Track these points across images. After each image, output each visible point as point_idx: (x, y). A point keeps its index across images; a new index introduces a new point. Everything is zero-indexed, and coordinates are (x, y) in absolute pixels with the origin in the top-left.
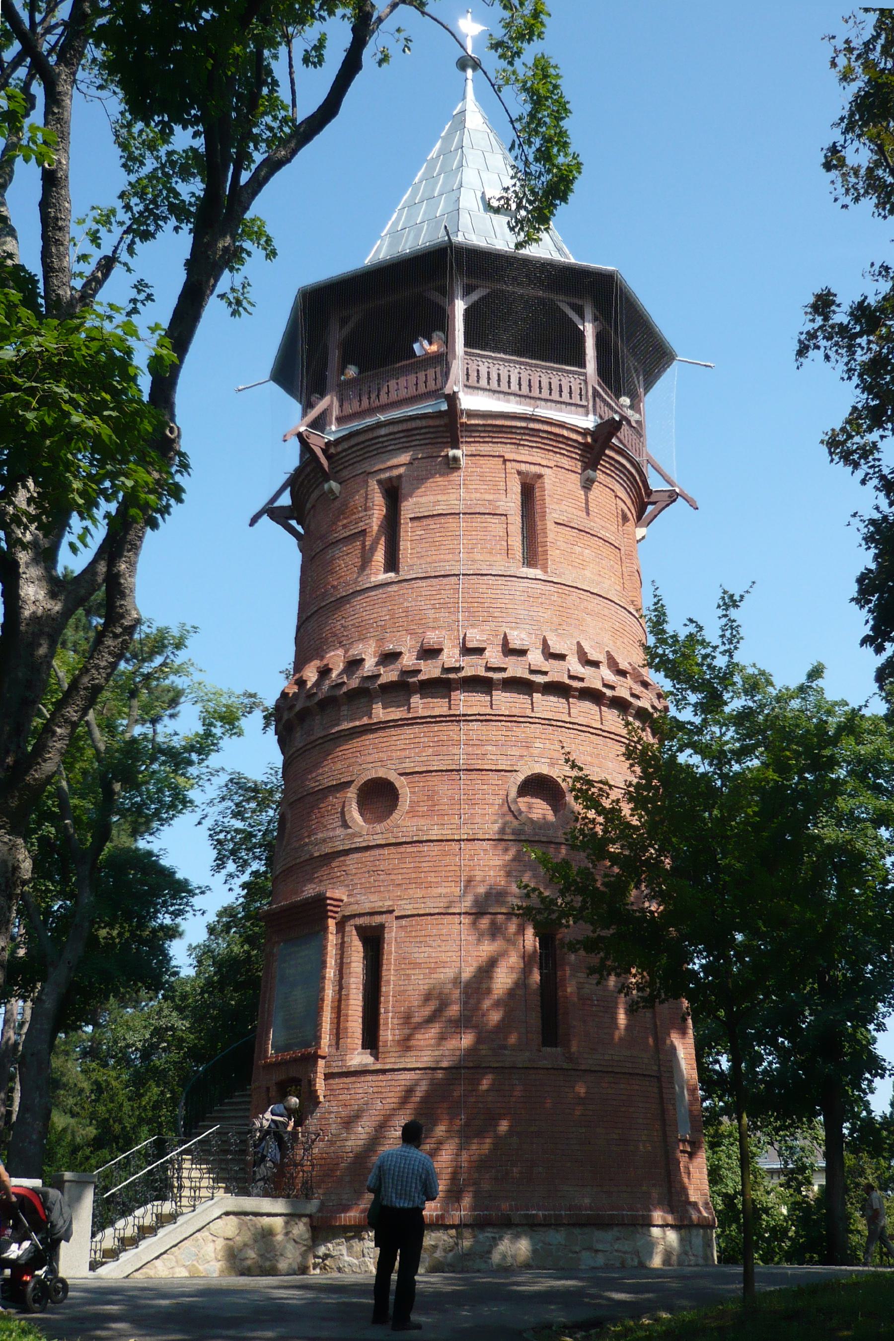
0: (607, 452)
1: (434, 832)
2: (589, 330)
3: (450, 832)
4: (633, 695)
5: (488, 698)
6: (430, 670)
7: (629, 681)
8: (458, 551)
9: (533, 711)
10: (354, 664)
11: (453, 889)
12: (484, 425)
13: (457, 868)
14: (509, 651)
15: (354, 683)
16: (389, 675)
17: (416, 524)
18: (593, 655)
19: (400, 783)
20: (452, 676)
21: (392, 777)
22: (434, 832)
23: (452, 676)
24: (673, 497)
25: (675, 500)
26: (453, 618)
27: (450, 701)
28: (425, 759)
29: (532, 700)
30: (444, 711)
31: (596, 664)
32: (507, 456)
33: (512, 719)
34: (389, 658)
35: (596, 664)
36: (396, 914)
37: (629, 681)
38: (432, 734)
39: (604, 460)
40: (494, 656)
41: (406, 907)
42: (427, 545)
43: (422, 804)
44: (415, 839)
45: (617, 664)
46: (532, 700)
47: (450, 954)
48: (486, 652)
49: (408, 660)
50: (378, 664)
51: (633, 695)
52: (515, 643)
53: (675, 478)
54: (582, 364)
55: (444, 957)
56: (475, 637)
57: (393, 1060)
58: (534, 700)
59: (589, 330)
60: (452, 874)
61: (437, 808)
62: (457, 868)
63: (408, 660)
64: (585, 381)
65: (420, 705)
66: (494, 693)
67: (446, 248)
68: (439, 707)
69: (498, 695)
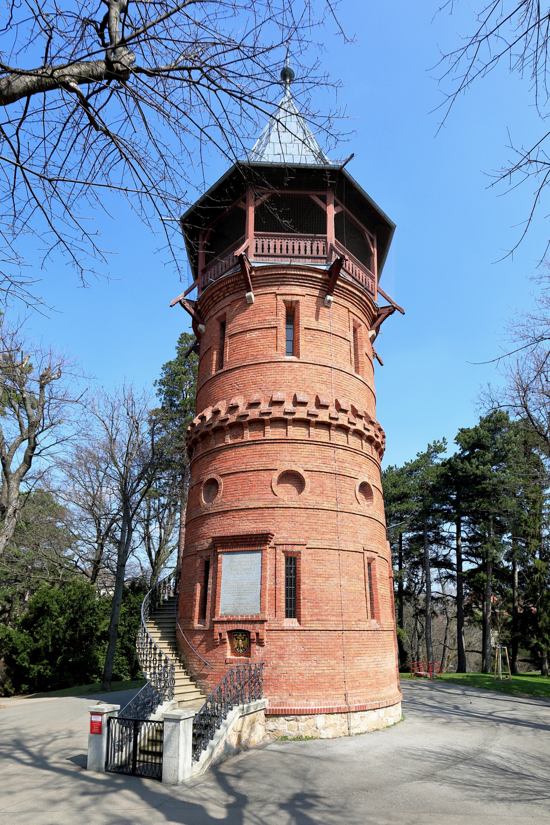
0: (338, 282)
1: (324, 505)
2: (331, 212)
3: (332, 506)
4: (365, 429)
5: (285, 430)
6: (254, 414)
7: (364, 421)
8: (330, 354)
9: (330, 440)
10: (216, 413)
11: (334, 537)
12: (343, 287)
13: (335, 526)
14: (297, 403)
15: (216, 423)
16: (232, 418)
17: (307, 332)
18: (343, 407)
19: (305, 475)
20: (266, 418)
21: (301, 471)
22: (324, 505)
23: (266, 418)
24: (392, 310)
25: (393, 312)
26: (328, 391)
27: (264, 432)
28: (318, 464)
29: (330, 433)
30: (327, 440)
31: (345, 411)
32: (351, 309)
33: (254, 443)
34: (233, 408)
35: (345, 411)
36: (307, 546)
37: (364, 421)
38: (320, 452)
39: (336, 288)
40: (288, 406)
41: (312, 543)
42: (314, 346)
43: (317, 489)
44: (315, 507)
45: (356, 411)
46: (330, 433)
47: (334, 571)
48: (285, 403)
49: (242, 410)
50: (227, 413)
51: (365, 429)
52: (300, 398)
53: (393, 299)
54: (324, 231)
55: (332, 572)
56: (278, 396)
57: (309, 625)
58: (331, 434)
59: (331, 212)
60: (333, 528)
61: (325, 492)
62: (335, 526)
63: (242, 410)
64: (326, 242)
65: (248, 435)
66: (288, 427)
67: (236, 168)
68: (258, 435)
69: (268, 429)
